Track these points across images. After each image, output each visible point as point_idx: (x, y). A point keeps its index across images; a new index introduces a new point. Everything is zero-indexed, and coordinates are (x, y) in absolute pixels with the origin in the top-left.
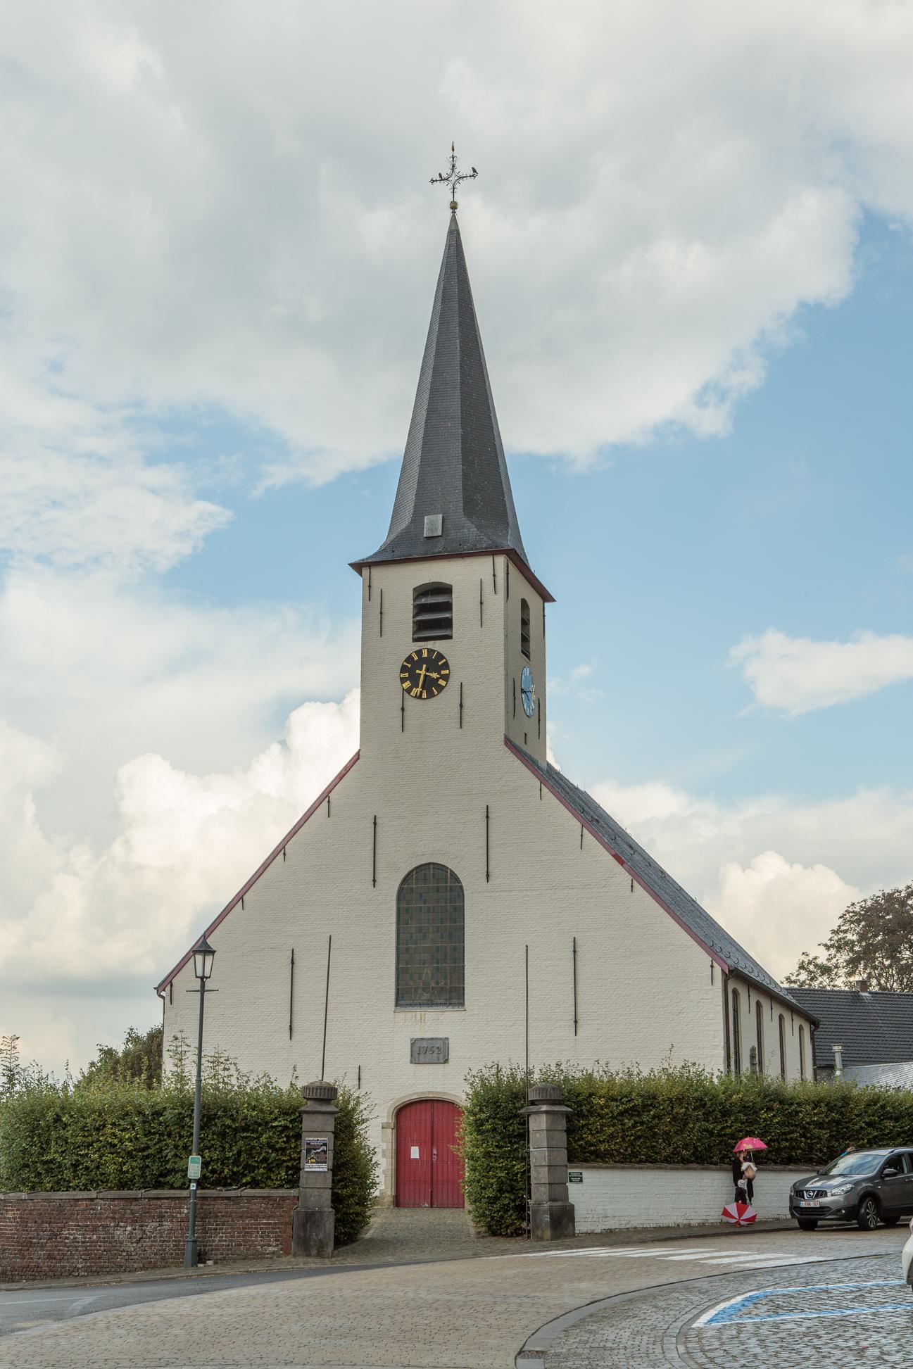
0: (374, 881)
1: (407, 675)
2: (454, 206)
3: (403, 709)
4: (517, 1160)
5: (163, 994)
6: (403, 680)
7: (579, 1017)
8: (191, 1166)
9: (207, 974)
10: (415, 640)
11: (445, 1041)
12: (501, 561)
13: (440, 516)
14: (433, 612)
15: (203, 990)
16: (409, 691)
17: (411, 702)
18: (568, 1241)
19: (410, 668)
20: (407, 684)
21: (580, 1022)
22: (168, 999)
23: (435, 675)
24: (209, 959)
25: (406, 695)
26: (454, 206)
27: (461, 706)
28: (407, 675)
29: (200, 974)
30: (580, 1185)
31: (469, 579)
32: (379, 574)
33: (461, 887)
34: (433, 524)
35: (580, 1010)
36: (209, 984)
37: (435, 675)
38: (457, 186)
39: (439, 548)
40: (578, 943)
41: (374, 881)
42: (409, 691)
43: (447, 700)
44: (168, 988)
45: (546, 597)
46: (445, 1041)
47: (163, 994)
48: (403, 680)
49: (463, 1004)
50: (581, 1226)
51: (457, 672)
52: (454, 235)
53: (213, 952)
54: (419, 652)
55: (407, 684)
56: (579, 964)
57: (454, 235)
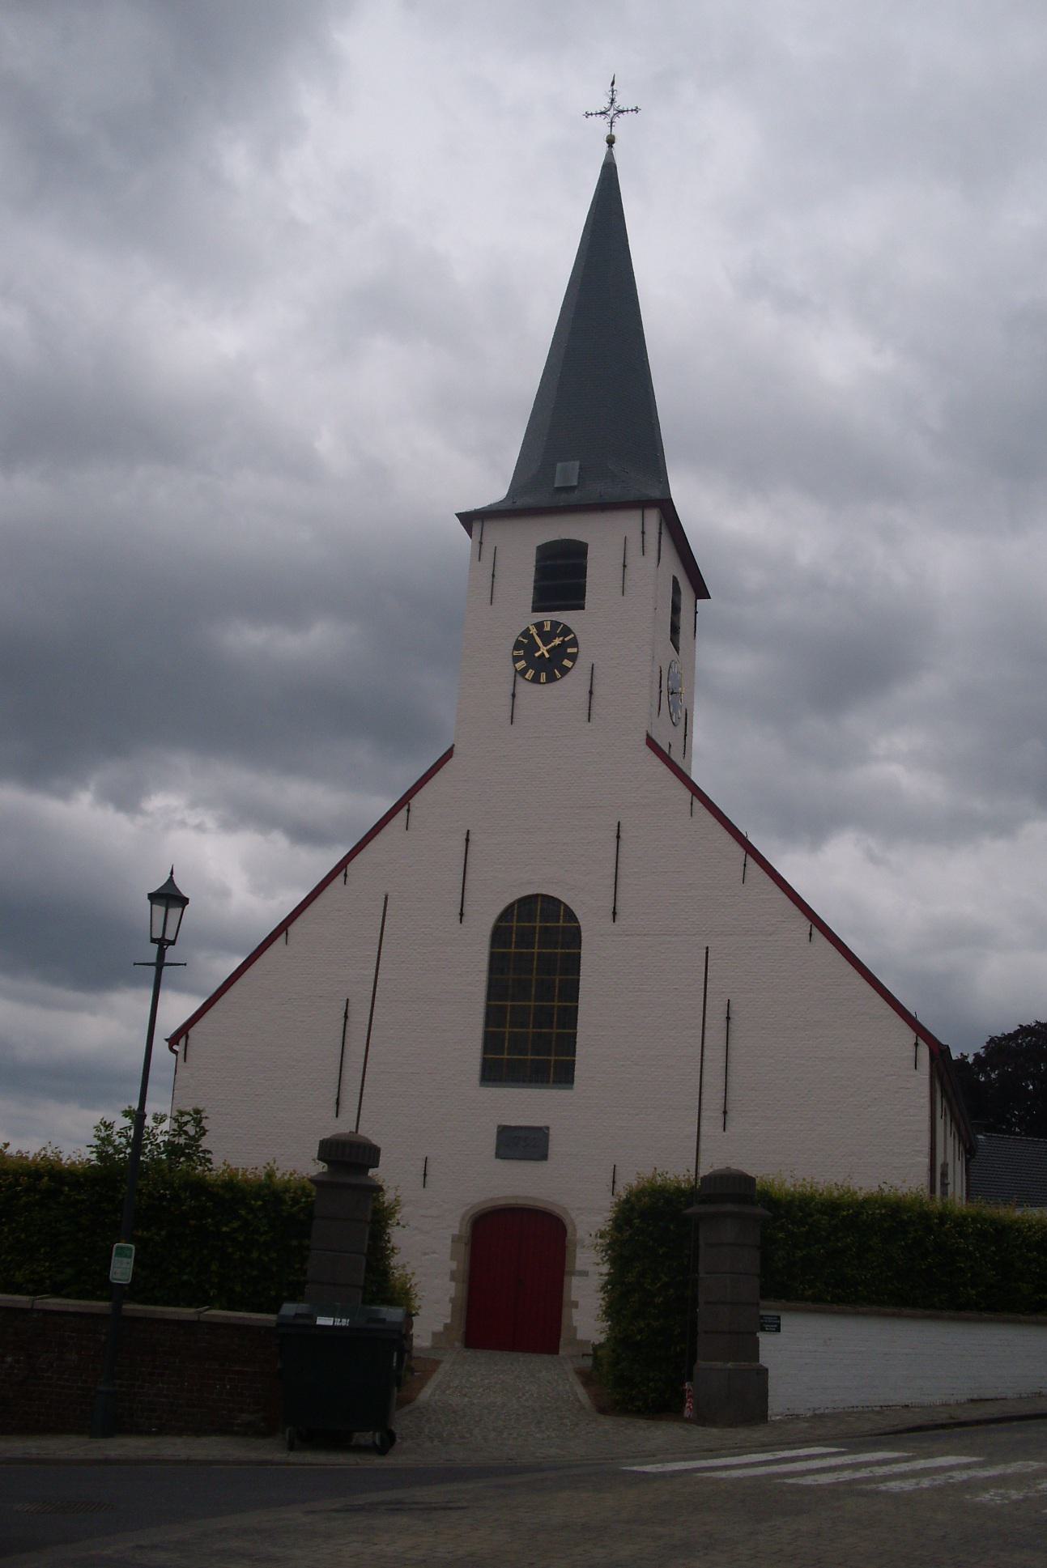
0: (462, 914)
1: (522, 652)
2: (611, 141)
3: (514, 695)
4: (708, 1275)
5: (175, 1047)
6: (516, 659)
7: (729, 1107)
8: (115, 1261)
9: (170, 936)
10: (535, 610)
11: (499, 1155)
12: (653, 517)
13: (577, 463)
14: (561, 578)
15: (160, 963)
16: (523, 672)
17: (524, 687)
18: (758, 1434)
19: (524, 646)
20: (521, 664)
21: (730, 1114)
22: (181, 1055)
23: (557, 641)
24: (174, 913)
25: (519, 678)
26: (611, 141)
27: (591, 692)
28: (522, 652)
29: (158, 935)
30: (777, 1335)
31: (607, 540)
32: (496, 533)
33: (578, 928)
34: (568, 472)
35: (731, 1096)
36: (171, 954)
37: (557, 641)
38: (616, 119)
39: (574, 498)
40: (733, 1008)
41: (462, 914)
42: (523, 672)
43: (573, 684)
44: (182, 1041)
45: (701, 592)
46: (499, 1155)
47: (175, 1047)
48: (516, 659)
49: (572, 1082)
50: (779, 1400)
51: (587, 652)
52: (609, 174)
53: (183, 901)
54: (539, 626)
55: (521, 664)
56: (732, 1035)
57: (609, 174)
